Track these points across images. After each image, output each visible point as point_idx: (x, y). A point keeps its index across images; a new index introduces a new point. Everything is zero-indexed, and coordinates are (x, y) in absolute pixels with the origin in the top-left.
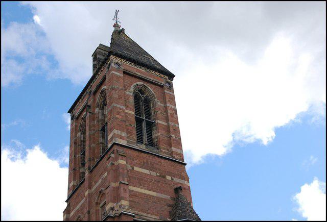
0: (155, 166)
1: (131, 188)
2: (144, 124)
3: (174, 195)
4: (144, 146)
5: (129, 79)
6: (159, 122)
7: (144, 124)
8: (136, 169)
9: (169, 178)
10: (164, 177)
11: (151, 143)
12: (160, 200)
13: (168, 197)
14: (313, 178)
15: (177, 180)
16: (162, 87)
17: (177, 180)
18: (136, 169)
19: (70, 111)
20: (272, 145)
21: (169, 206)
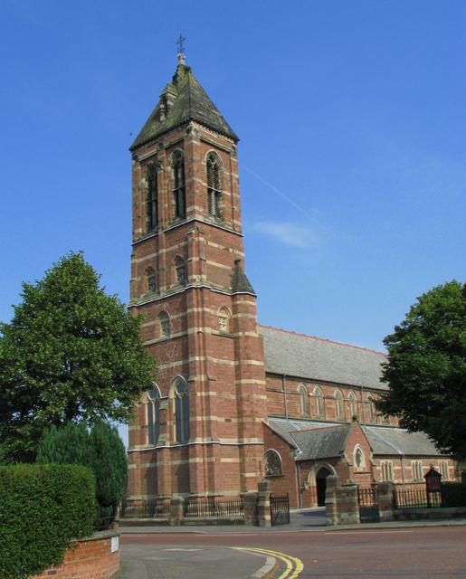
0: (180, 170)
1: (208, 262)
2: (213, 194)
3: (234, 266)
4: (213, 219)
5: (205, 146)
6: (225, 192)
7: (213, 194)
8: (210, 243)
9: (231, 250)
10: (227, 249)
11: (219, 215)
12: (224, 270)
13: (230, 268)
14: (394, 388)
15: (237, 252)
16: (228, 153)
17: (237, 252)
18: (210, 243)
19: (132, 150)
20: (441, 484)
21: (230, 276)
